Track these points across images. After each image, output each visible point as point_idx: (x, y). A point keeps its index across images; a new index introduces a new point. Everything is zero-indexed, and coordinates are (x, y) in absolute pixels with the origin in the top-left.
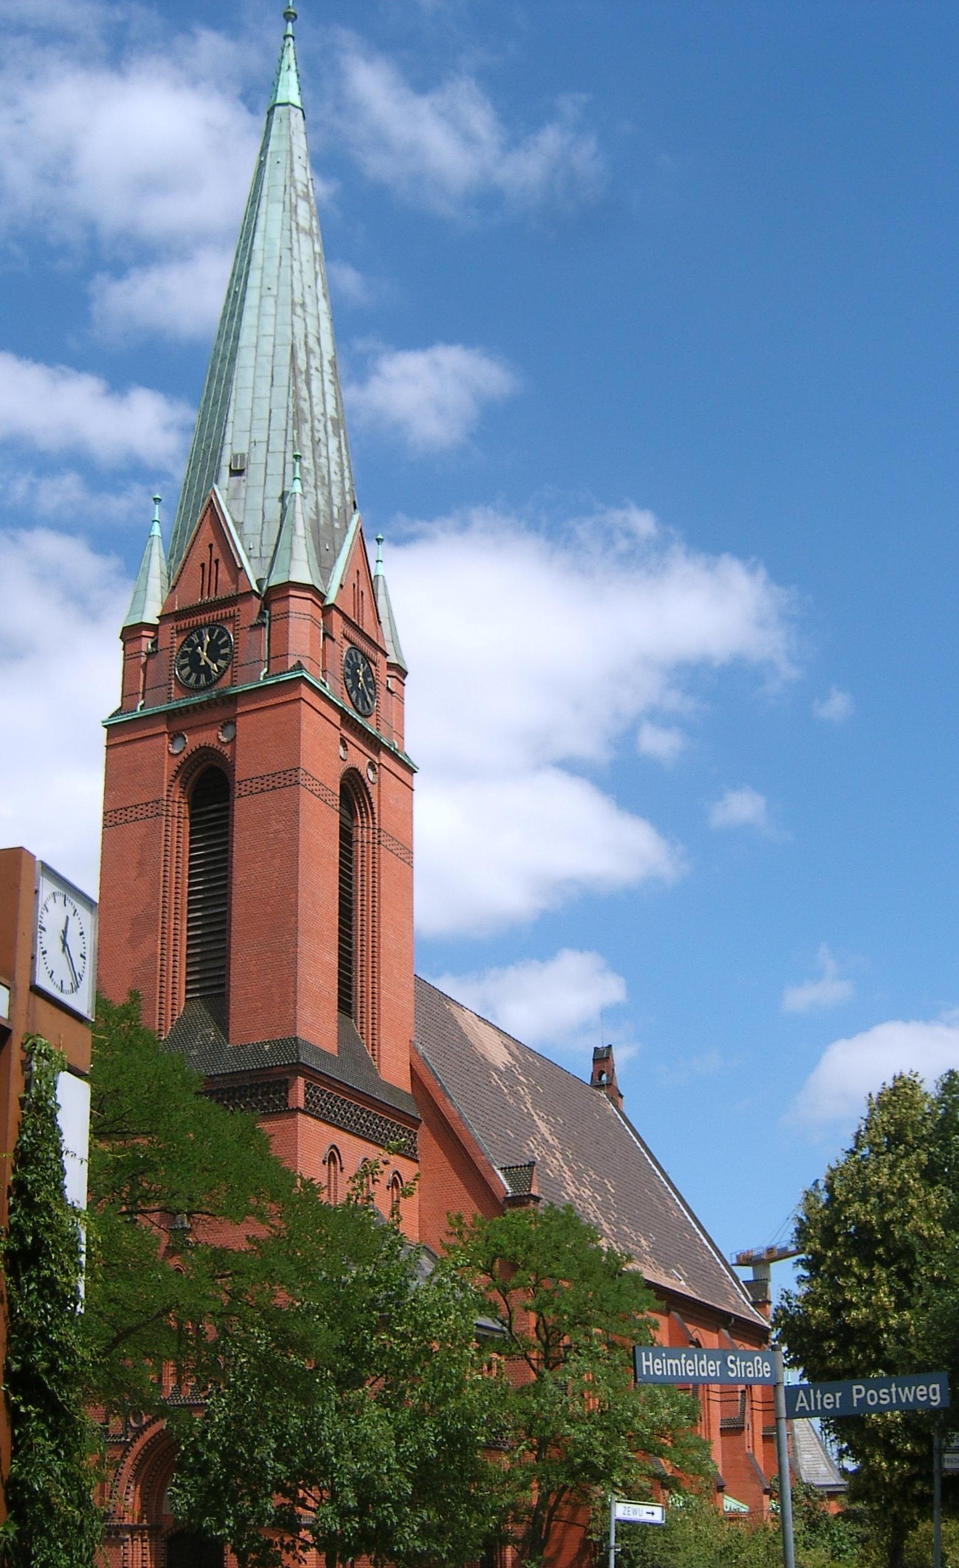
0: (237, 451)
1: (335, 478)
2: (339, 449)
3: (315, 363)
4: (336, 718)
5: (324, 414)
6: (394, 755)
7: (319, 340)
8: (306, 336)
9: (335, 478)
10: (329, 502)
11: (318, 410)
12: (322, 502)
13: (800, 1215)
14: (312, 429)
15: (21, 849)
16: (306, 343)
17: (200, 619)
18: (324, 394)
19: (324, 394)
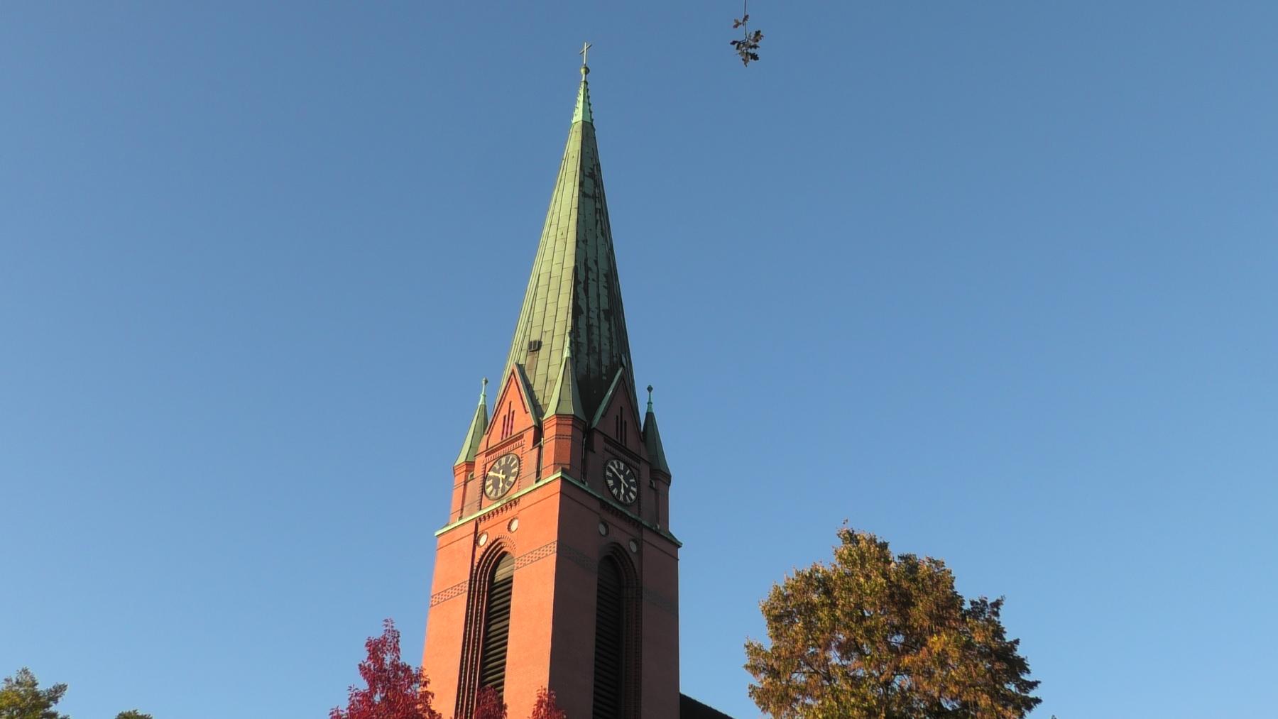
0: (532, 339)
1: (606, 347)
2: (609, 329)
3: (591, 276)
4: (596, 506)
5: (599, 308)
6: (657, 533)
7: (596, 262)
8: (586, 260)
9: (606, 347)
10: (599, 363)
11: (593, 306)
12: (593, 365)
13: (748, 662)
14: (588, 317)
15: (666, 478)
16: (586, 264)
17: (501, 452)
18: (598, 295)
19: (598, 295)
